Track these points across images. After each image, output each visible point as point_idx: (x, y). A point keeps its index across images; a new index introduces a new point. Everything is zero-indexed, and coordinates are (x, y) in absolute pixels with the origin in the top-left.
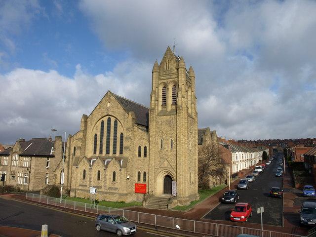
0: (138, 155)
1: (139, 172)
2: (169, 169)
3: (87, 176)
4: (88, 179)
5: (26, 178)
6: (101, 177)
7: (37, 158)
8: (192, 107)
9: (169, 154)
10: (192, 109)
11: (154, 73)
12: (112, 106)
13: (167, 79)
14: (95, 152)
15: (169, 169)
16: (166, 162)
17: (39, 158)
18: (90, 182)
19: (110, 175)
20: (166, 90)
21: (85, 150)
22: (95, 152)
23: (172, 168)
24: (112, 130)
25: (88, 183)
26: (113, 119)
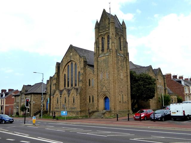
0: (88, 85)
1: (90, 96)
2: (106, 92)
3: (59, 102)
4: (60, 104)
5: (18, 108)
6: (66, 101)
7: (34, 95)
8: (124, 49)
9: (106, 82)
10: (124, 51)
11: (110, 24)
12: (73, 55)
13: (104, 32)
14: (65, 86)
15: (106, 92)
16: (104, 88)
17: (36, 95)
18: (61, 105)
19: (71, 100)
20: (104, 39)
21: (59, 85)
22: (65, 86)
23: (108, 91)
24: (74, 70)
25: (60, 106)
26: (74, 63)
